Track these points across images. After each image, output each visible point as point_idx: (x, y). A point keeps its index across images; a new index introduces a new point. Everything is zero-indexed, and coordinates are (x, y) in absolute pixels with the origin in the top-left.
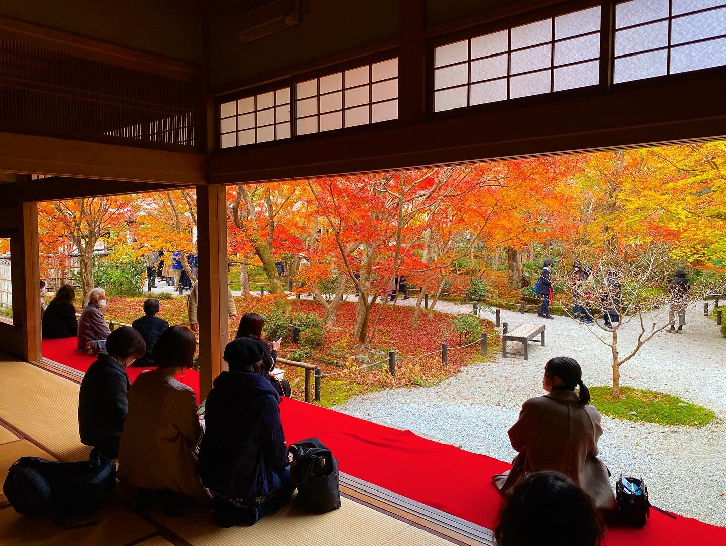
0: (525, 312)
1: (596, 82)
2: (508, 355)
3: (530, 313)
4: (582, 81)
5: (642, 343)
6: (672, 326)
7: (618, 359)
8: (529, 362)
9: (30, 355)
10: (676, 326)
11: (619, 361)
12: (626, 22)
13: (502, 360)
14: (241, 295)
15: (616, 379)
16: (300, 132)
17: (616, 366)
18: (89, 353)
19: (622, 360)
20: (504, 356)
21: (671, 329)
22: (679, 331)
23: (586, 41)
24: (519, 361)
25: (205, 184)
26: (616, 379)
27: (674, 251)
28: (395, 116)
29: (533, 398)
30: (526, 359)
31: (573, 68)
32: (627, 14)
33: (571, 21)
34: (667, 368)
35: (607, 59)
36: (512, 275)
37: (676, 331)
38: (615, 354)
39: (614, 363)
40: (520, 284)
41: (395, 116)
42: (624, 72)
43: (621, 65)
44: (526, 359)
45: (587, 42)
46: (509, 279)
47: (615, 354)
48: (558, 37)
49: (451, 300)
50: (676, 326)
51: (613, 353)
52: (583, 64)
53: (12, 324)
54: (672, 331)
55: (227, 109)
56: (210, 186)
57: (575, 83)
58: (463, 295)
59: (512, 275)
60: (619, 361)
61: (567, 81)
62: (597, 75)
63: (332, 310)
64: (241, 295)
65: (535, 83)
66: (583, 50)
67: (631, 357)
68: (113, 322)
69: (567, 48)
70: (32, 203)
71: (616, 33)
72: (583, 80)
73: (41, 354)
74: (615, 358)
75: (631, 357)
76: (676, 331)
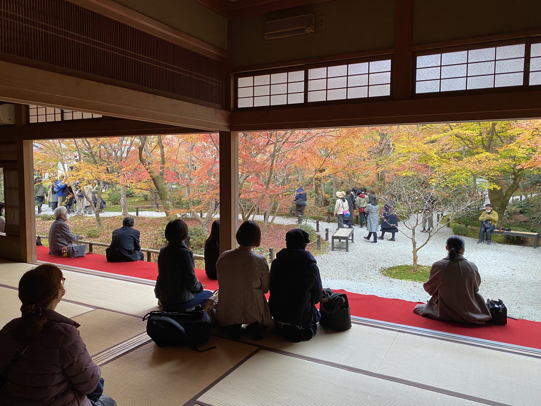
0: (331, 222)
1: (521, 84)
2: (335, 249)
3: (333, 222)
4: (512, 82)
5: (431, 236)
6: (424, 228)
7: (416, 246)
8: (350, 253)
9: (29, 258)
10: (427, 228)
11: (417, 248)
12: (536, 54)
13: (331, 252)
14: (121, 215)
15: (415, 260)
16: (310, 100)
17: (415, 252)
18: (64, 255)
19: (418, 247)
20: (333, 250)
21: (424, 230)
22: (428, 231)
23: (515, 62)
24: (343, 252)
25: (229, 131)
26: (415, 260)
27: (432, 180)
28: (388, 94)
29: (435, 263)
30: (347, 251)
31: (507, 75)
32: (537, 50)
33: (506, 50)
34: (432, 253)
35: (527, 72)
36: (318, 198)
37: (427, 232)
38: (414, 244)
39: (414, 249)
40: (323, 203)
41: (388, 94)
42: (535, 80)
43: (533, 76)
44: (347, 251)
45: (515, 63)
46: (316, 200)
47: (414, 244)
48: (498, 58)
49: (280, 215)
50: (427, 228)
51: (413, 243)
52: (513, 74)
53: (5, 235)
54: (424, 231)
55: (242, 82)
56: (232, 132)
57: (508, 83)
58: (287, 212)
59: (318, 198)
60: (417, 248)
61: (502, 82)
62: (521, 80)
63: (205, 223)
64: (121, 215)
65: (483, 81)
66: (513, 66)
67: (424, 245)
68: (40, 236)
69: (504, 64)
70: (30, 141)
71: (531, 59)
72: (513, 82)
73: (36, 257)
74: (414, 246)
75: (424, 245)
76: (427, 232)
